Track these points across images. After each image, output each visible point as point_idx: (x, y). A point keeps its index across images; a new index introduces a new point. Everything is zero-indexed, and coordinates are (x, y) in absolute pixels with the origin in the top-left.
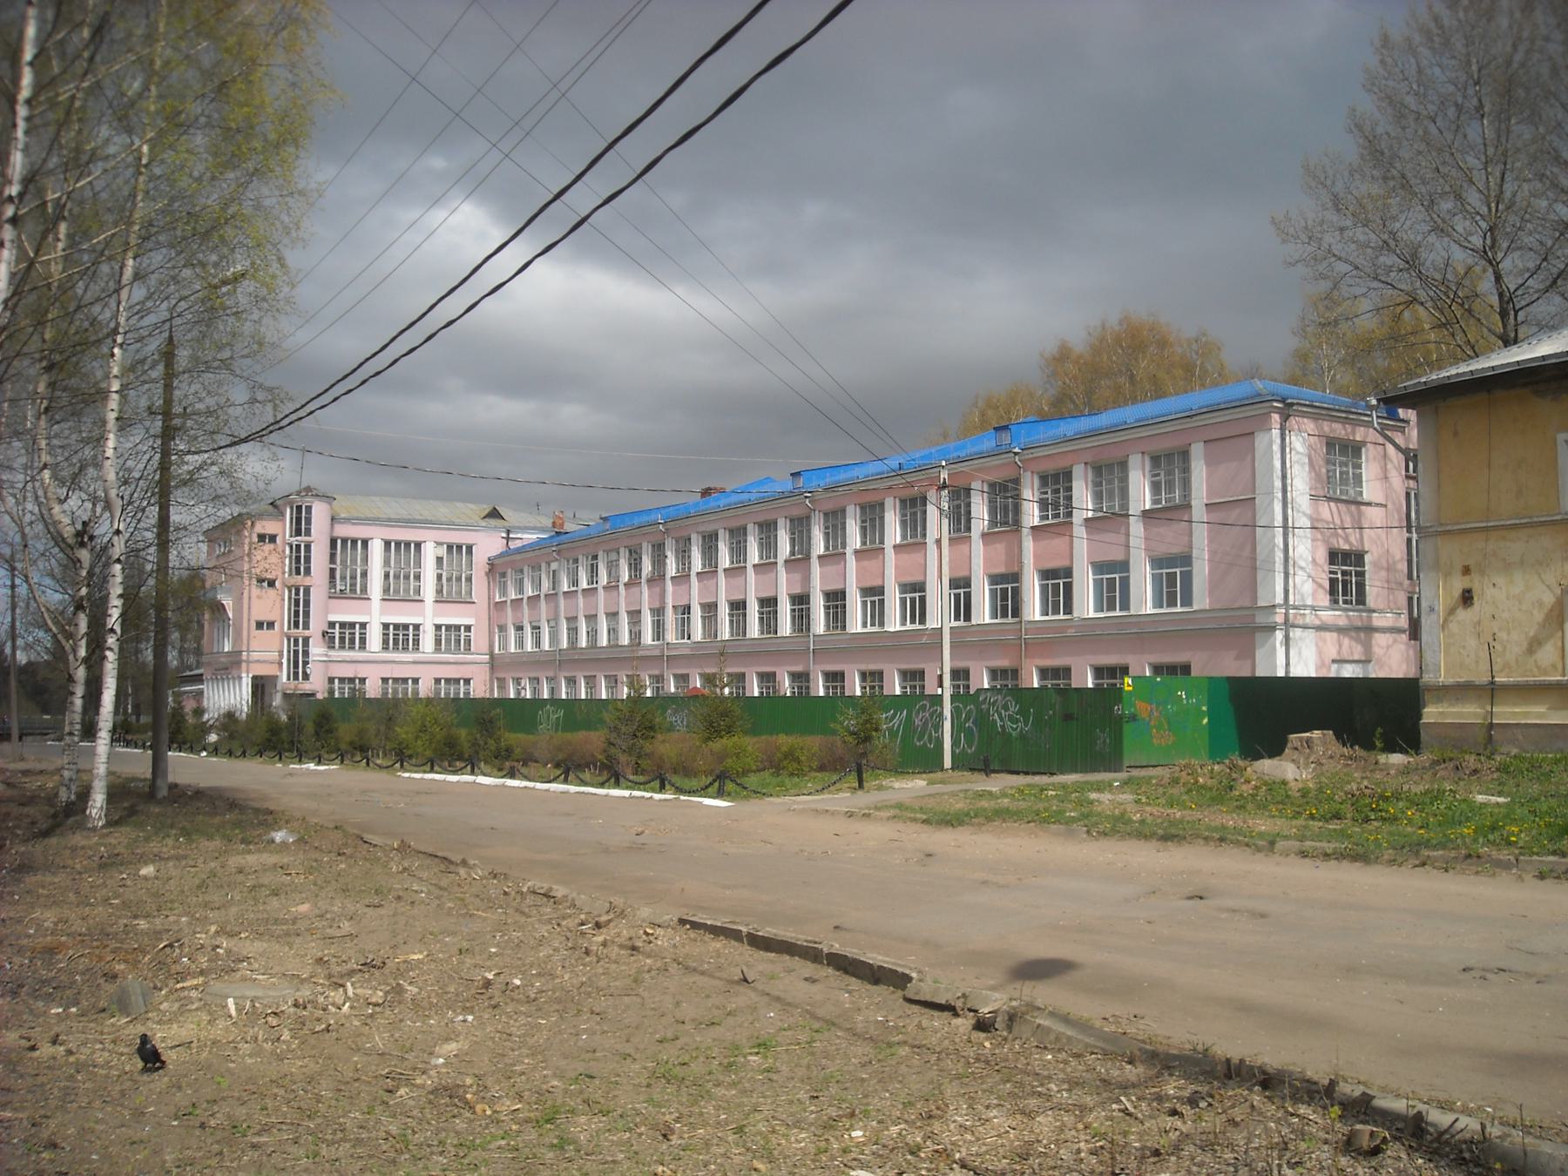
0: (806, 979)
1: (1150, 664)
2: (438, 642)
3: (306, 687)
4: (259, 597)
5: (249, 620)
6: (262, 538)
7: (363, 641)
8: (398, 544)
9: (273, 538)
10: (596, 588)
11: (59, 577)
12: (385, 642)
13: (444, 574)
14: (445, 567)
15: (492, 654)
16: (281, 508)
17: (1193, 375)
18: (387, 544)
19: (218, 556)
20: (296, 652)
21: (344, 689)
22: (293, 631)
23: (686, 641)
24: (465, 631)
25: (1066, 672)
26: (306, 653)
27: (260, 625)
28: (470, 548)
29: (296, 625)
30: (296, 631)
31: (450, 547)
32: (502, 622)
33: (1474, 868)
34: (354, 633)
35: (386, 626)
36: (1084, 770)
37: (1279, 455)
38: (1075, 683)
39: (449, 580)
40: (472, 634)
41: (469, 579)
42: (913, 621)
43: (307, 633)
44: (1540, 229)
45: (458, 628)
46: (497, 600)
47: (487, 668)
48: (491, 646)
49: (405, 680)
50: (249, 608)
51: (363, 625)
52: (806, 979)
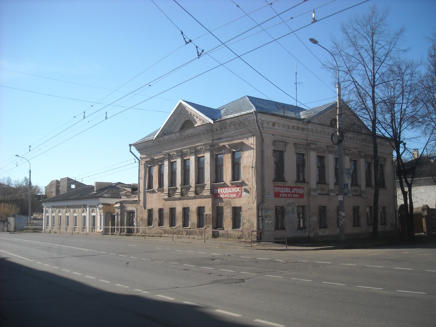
36: (322, 263)
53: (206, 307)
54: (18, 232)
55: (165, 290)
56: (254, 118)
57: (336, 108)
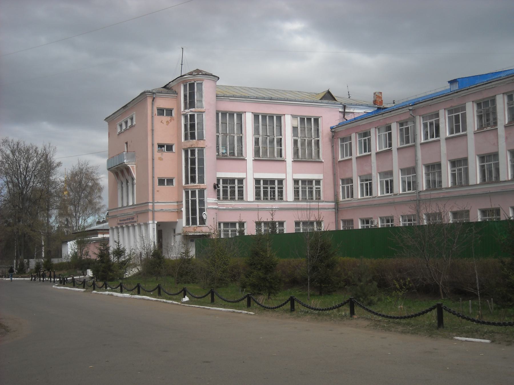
1: (480, 210)
2: (296, 193)
3: (204, 230)
4: (160, 159)
5: (153, 177)
6: (161, 111)
7: (241, 193)
8: (264, 117)
9: (169, 112)
10: (351, 159)
12: (258, 194)
13: (299, 141)
14: (299, 135)
15: (336, 201)
16: (174, 89)
18: (256, 116)
19: (120, 134)
20: (194, 202)
21: (228, 231)
22: (190, 185)
23: (389, 194)
24: (316, 185)
25: (498, 211)
26: (202, 202)
27: (161, 182)
28: (316, 120)
29: (193, 180)
30: (193, 184)
31: (302, 120)
32: (347, 176)
34: (234, 187)
35: (257, 181)
38: (472, 220)
39: (303, 144)
40: (321, 187)
41: (317, 143)
42: (348, 197)
43: (202, 186)
45: (310, 182)
46: (340, 159)
47: (332, 213)
48: (336, 195)
49: (233, 224)
50: (153, 168)
51: (241, 181)
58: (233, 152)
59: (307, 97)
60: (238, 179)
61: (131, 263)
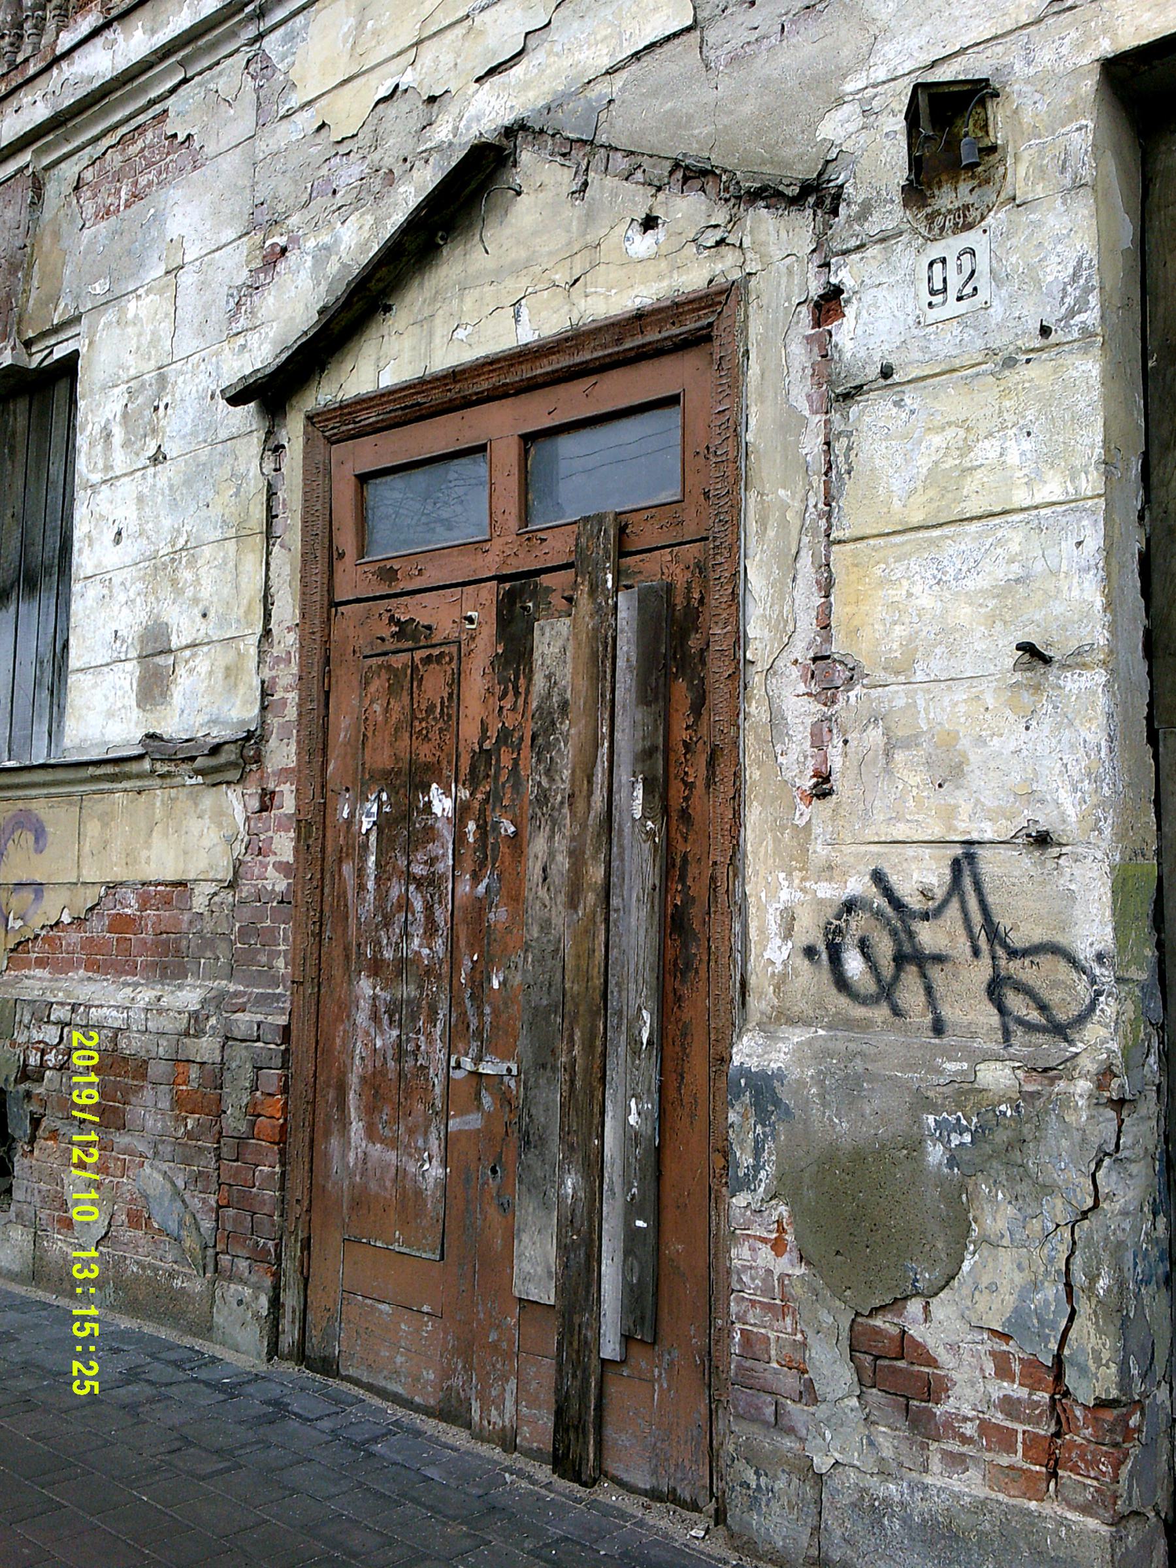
0: (517, 321)
11: (226, 1397)
17: (933, 212)
33: (47, 241)
37: (164, 36)
44: (120, 693)
52: (517, 321)
53: (421, 285)
54: (742, 829)
55: (880, 689)
56: (276, 1077)
57: (421, 782)
58: (261, 1068)
59: (631, 970)
60: (934, 90)
61: (403, 1327)
